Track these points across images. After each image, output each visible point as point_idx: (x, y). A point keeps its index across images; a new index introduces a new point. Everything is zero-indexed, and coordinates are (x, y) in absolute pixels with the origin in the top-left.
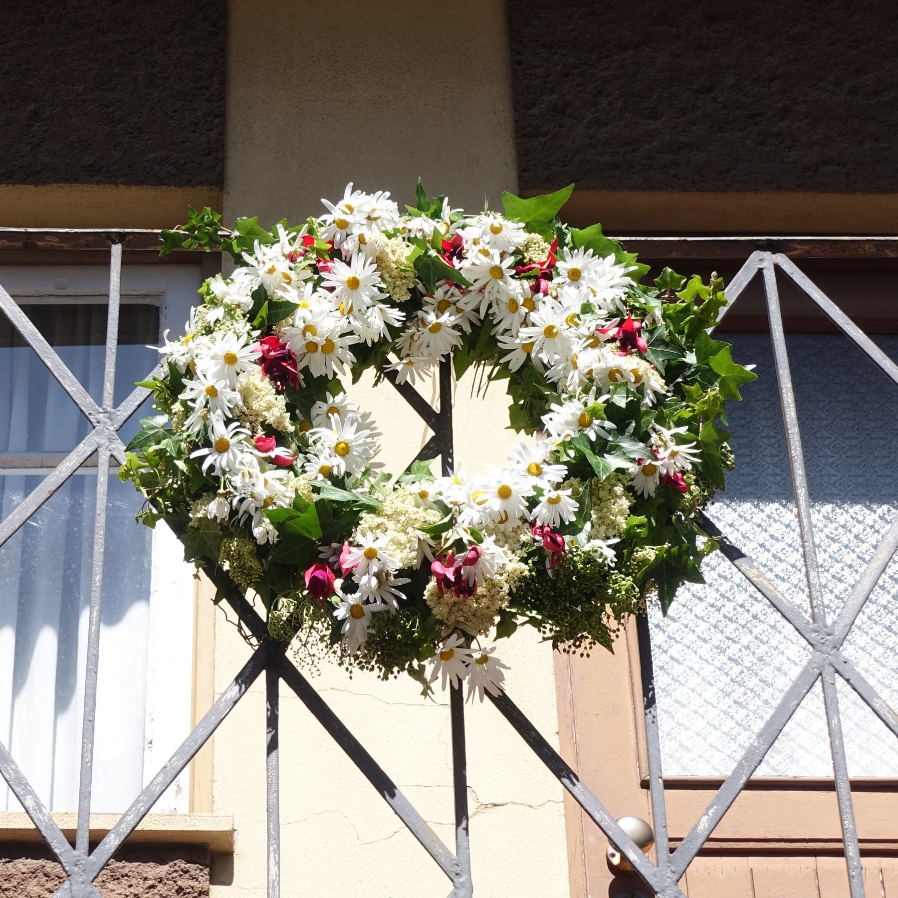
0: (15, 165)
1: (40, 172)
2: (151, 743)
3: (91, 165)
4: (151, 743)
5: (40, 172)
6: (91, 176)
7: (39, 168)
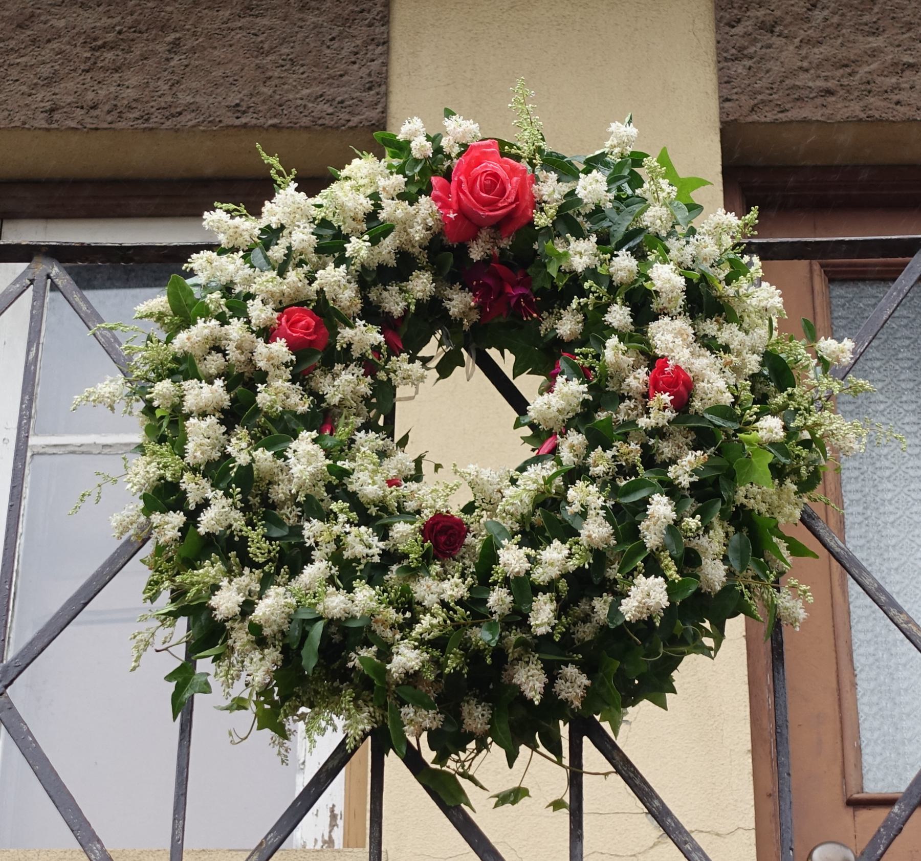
0: (152, 107)
1: (180, 114)
2: (304, 763)
3: (237, 105)
4: (304, 763)
5: (180, 114)
6: (237, 118)
7: (178, 110)
